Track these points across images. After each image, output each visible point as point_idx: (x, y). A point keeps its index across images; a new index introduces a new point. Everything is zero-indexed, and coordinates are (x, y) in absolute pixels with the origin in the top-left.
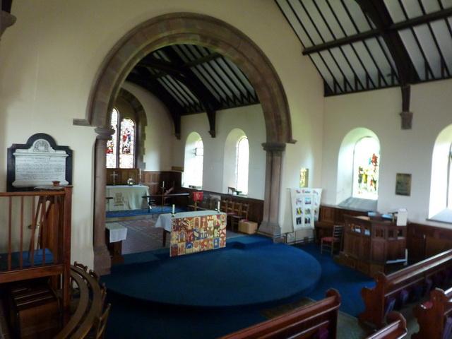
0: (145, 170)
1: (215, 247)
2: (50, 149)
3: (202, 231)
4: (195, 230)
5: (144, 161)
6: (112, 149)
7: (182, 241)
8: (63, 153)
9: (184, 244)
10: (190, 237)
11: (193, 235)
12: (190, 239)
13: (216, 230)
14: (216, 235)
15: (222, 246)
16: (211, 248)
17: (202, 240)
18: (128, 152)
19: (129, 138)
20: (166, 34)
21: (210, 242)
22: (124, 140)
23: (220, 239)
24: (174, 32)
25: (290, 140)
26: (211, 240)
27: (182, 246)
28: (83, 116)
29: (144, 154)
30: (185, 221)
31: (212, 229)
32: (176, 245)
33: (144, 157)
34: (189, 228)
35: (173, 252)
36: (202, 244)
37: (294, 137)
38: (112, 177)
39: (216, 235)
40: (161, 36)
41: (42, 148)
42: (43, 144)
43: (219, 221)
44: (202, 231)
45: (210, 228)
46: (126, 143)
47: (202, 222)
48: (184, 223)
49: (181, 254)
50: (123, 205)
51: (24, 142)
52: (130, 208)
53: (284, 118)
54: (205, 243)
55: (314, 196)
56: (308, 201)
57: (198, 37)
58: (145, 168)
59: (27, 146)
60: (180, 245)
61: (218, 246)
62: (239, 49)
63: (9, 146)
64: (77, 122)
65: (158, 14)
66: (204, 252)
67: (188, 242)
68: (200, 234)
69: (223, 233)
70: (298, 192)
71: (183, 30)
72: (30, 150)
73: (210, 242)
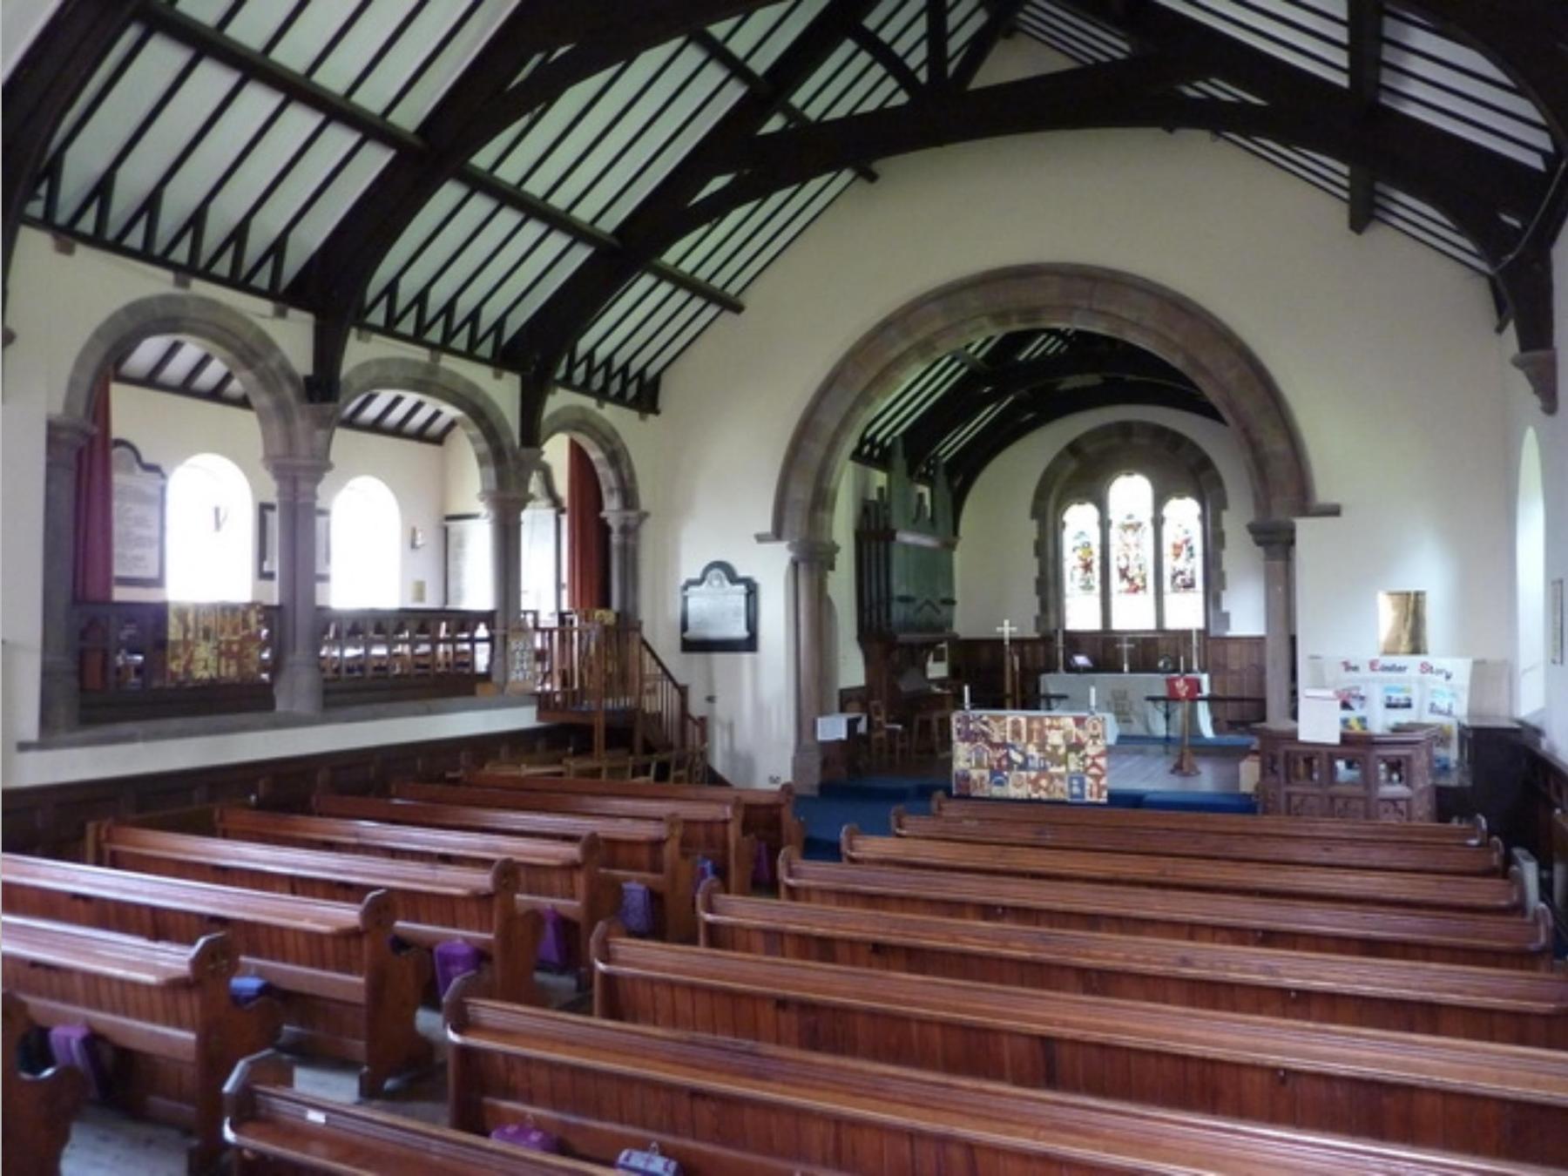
0: (1229, 634)
1: (1073, 796)
2: (726, 583)
3: (1032, 750)
4: (1013, 747)
5: (1225, 608)
6: (1144, 580)
7: (979, 765)
8: (742, 588)
9: (986, 773)
10: (999, 761)
11: (1007, 756)
12: (1000, 765)
13: (1072, 756)
14: (1073, 767)
15: (1094, 799)
16: (1058, 796)
17: (1033, 774)
18: (1189, 586)
19: (1191, 549)
20: (903, 346)
21: (1057, 782)
22: (1177, 556)
23: (1089, 781)
24: (919, 336)
25: (1305, 504)
26: (1060, 777)
27: (982, 778)
28: (767, 526)
29: (1223, 587)
30: (986, 723)
31: (1062, 751)
32: (965, 771)
33: (1224, 595)
34: (996, 739)
35: (959, 786)
36: (1035, 783)
37: (1324, 493)
38: (1121, 649)
39: (1073, 767)
40: (894, 353)
41: (716, 583)
42: (719, 577)
43: (1081, 733)
44: (1032, 750)
45: (1055, 747)
46: (1180, 564)
47: (1030, 732)
48: (985, 728)
49: (980, 794)
50: (1130, 721)
51: (697, 575)
52: (1148, 728)
53: (1279, 446)
54: (1044, 782)
55: (1421, 682)
56: (1399, 696)
57: (985, 321)
58: (1227, 627)
59: (699, 582)
60: (975, 774)
61: (1082, 796)
62: (1095, 306)
63: (683, 582)
64: (761, 538)
65: (878, 319)
66: (1039, 801)
67: (994, 773)
68: (1026, 758)
69: (1094, 765)
70: (1348, 667)
71: (939, 324)
72: (704, 587)
73: (1057, 782)
